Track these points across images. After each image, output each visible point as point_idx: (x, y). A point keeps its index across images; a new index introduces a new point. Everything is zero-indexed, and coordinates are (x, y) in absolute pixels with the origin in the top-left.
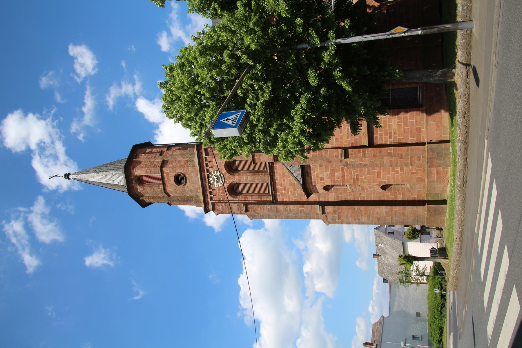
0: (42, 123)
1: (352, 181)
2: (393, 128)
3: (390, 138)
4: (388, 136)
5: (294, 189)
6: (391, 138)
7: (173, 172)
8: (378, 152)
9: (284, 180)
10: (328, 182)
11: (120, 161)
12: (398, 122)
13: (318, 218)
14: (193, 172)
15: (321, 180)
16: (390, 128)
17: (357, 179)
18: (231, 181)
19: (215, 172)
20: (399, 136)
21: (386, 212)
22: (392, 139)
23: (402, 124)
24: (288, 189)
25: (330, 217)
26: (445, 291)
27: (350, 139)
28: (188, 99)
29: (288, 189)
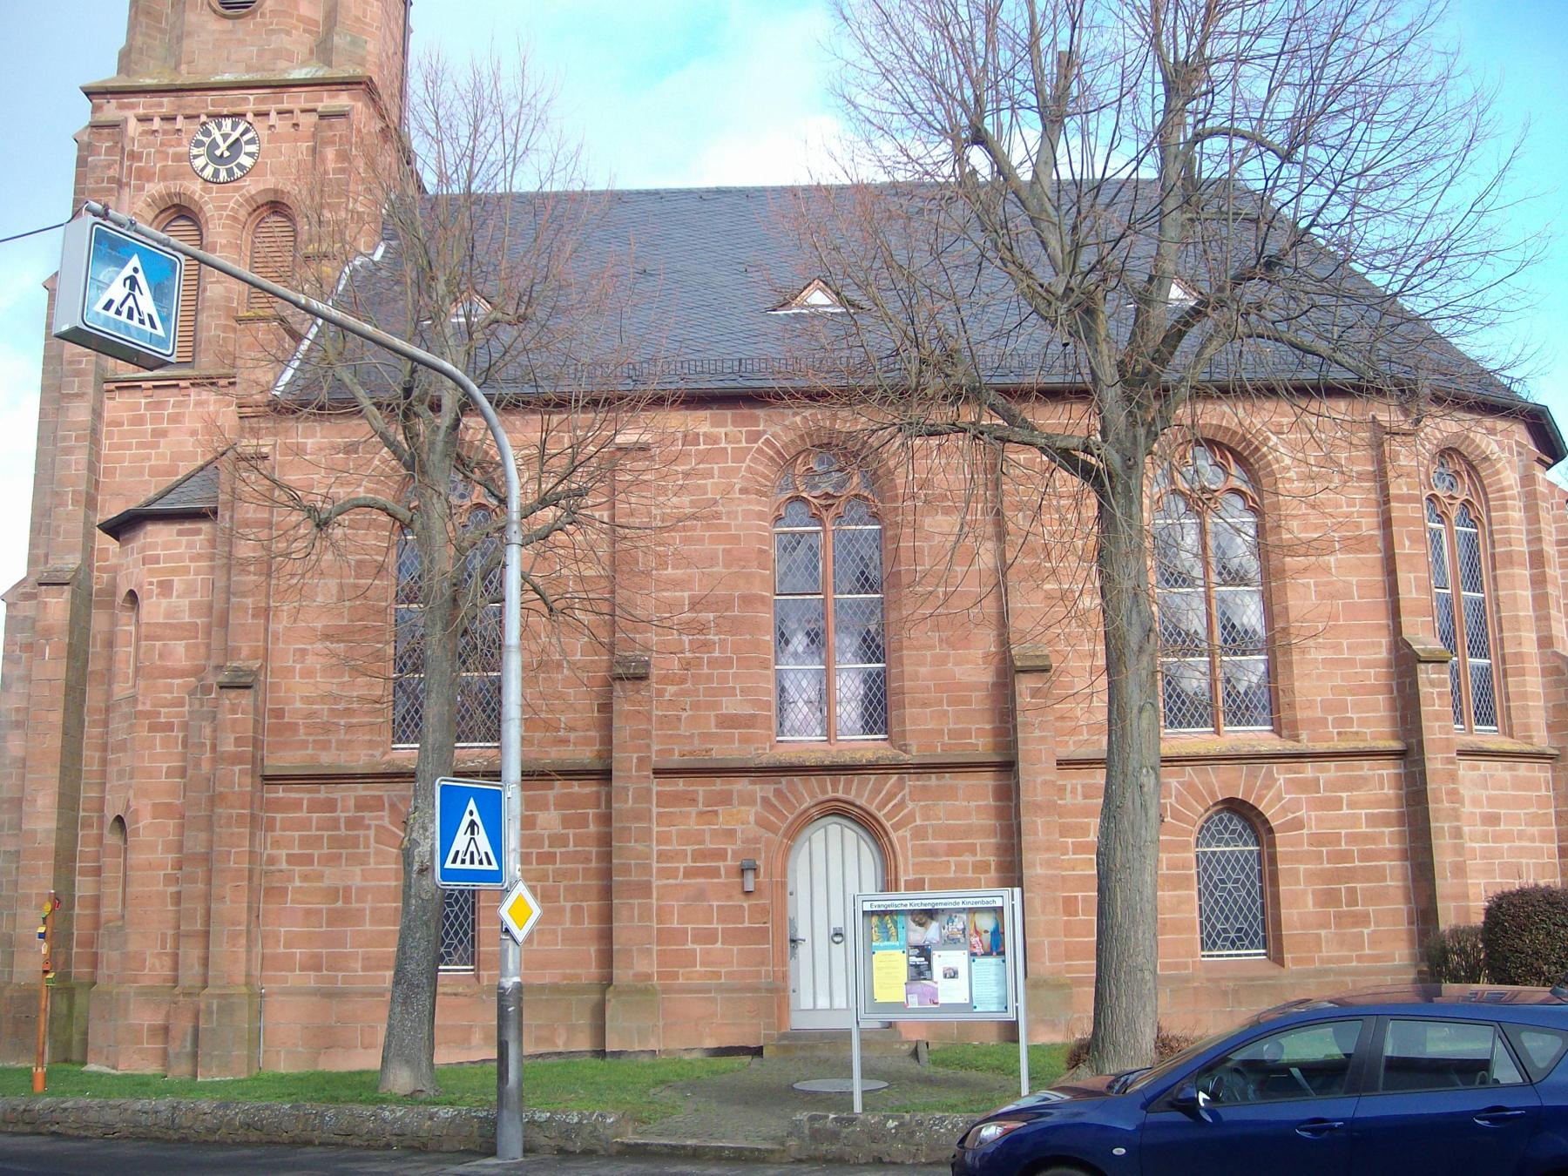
0: (1409, 988)
1: (148, 707)
2: (327, 870)
3: (291, 859)
4: (296, 851)
5: (154, 472)
6: (289, 862)
8: (234, 812)
9: (194, 433)
13: (32, 561)
14: (261, 53)
15: (161, 584)
18: (209, 210)
19: (252, 148)
20: (297, 890)
21: (33, 833)
22: (284, 866)
23: (340, 904)
24: (156, 446)
25: (27, 608)
27: (298, 705)
29: (156, 446)
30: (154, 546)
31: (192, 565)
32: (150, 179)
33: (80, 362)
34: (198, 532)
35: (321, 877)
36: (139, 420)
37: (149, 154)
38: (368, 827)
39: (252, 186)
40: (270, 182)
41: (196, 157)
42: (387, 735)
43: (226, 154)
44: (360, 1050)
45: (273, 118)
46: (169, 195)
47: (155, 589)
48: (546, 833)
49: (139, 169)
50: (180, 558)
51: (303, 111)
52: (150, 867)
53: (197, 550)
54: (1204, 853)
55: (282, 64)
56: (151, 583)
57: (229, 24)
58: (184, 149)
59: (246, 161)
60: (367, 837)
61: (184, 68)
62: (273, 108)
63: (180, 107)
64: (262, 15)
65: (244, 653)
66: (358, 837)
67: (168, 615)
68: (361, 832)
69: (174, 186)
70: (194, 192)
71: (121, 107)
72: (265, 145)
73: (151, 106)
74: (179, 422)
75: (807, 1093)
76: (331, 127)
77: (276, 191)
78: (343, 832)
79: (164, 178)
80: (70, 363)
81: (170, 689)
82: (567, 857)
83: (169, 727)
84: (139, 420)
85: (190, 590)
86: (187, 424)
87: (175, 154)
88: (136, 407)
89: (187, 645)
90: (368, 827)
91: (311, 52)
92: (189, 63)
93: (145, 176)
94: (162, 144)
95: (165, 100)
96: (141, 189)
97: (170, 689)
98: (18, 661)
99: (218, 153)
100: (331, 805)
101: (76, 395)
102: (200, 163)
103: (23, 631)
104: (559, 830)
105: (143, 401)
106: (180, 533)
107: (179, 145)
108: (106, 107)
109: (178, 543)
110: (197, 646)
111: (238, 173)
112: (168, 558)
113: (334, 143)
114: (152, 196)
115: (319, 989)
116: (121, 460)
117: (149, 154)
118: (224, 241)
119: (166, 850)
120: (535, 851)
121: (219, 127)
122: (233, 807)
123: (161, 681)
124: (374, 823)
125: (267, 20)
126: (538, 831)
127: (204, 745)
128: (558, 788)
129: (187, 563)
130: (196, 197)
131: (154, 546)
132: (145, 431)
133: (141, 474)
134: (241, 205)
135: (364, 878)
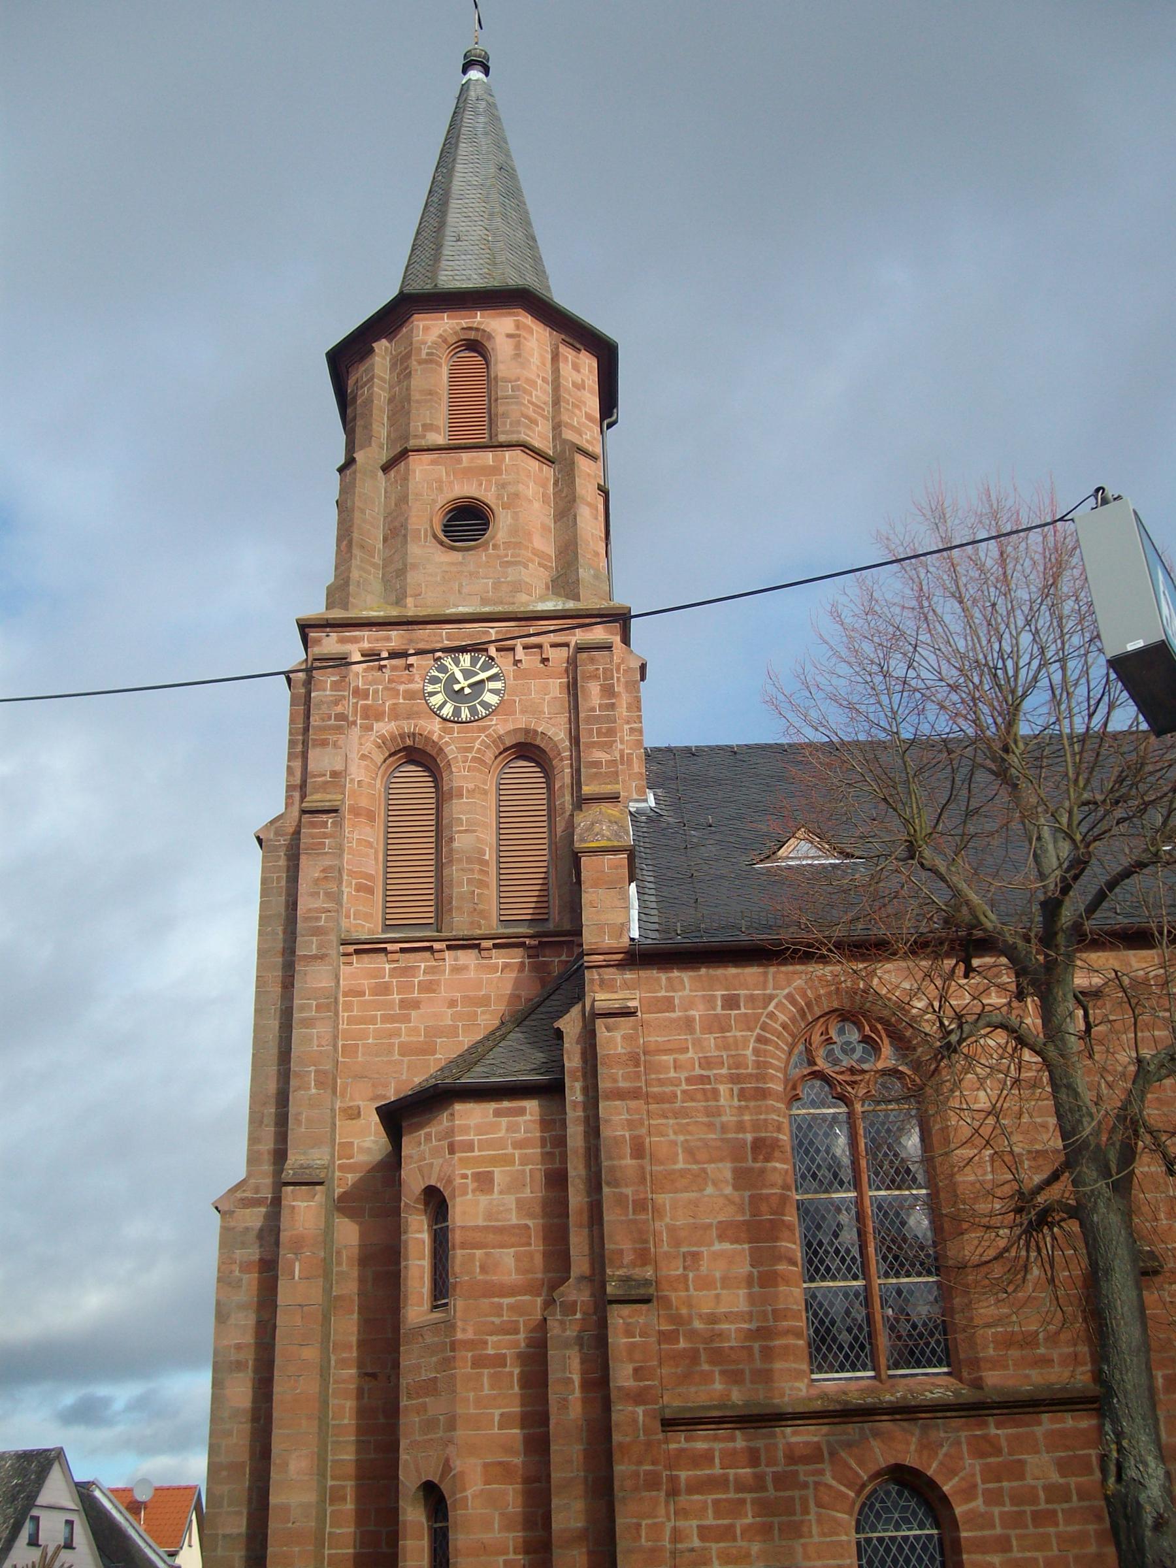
1: (470, 1335)
5: (405, 1050)
6: (702, 1538)
7: (499, 497)
9: (452, 1003)
10: (467, 1211)
11: (540, 271)
14: (497, 585)
15: (477, 1177)
18: (451, 751)
19: (498, 685)
21: (286, 1508)
22: (696, 1543)
26: (1101, 889)
28: (1046, 1230)
30: (465, 1129)
31: (517, 1152)
32: (379, 717)
33: (318, 919)
34: (522, 1112)
36: (384, 989)
37: (376, 692)
38: (805, 1485)
39: (501, 726)
40: (521, 721)
41: (432, 694)
43: (467, 691)
45: (520, 653)
46: (402, 736)
47: (471, 1184)
48: (1040, 1483)
49: (366, 709)
51: (553, 645)
52: (484, 1549)
53: (521, 1135)
54: (868, 1541)
55: (524, 598)
56: (465, 1176)
57: (458, 556)
58: (416, 686)
59: (492, 699)
61: (410, 601)
63: (411, 641)
64: (495, 547)
65: (628, 1258)
66: (792, 1498)
67: (489, 1216)
68: (796, 1493)
69: (408, 726)
70: (432, 732)
71: (342, 641)
72: (511, 682)
73: (377, 640)
74: (434, 991)
76: (592, 660)
77: (527, 731)
78: (771, 1493)
79: (395, 715)
80: (306, 919)
82: (1070, 1515)
83: (500, 1360)
84: (384, 989)
85: (515, 1185)
86: (444, 993)
87: (405, 691)
88: (379, 973)
91: (547, 588)
92: (416, 595)
93: (372, 715)
94: (390, 681)
95: (393, 633)
96: (370, 728)
98: (238, 1285)
99: (457, 687)
102: (436, 700)
103: (243, 1245)
104: (1055, 1478)
105: (387, 966)
106: (497, 1113)
107: (411, 681)
108: (325, 641)
109: (494, 1127)
110: (531, 1255)
111: (482, 711)
112: (483, 1145)
113: (597, 677)
114: (382, 737)
116: (364, 1035)
117: (376, 692)
118: (471, 786)
120: (1028, 1509)
121: (457, 662)
124: (811, 1479)
125: (502, 552)
126: (1029, 1481)
127: (570, 1380)
128: (1048, 1423)
129: (510, 1150)
130: (435, 738)
131: (465, 1129)
133: (390, 1052)
134: (488, 747)
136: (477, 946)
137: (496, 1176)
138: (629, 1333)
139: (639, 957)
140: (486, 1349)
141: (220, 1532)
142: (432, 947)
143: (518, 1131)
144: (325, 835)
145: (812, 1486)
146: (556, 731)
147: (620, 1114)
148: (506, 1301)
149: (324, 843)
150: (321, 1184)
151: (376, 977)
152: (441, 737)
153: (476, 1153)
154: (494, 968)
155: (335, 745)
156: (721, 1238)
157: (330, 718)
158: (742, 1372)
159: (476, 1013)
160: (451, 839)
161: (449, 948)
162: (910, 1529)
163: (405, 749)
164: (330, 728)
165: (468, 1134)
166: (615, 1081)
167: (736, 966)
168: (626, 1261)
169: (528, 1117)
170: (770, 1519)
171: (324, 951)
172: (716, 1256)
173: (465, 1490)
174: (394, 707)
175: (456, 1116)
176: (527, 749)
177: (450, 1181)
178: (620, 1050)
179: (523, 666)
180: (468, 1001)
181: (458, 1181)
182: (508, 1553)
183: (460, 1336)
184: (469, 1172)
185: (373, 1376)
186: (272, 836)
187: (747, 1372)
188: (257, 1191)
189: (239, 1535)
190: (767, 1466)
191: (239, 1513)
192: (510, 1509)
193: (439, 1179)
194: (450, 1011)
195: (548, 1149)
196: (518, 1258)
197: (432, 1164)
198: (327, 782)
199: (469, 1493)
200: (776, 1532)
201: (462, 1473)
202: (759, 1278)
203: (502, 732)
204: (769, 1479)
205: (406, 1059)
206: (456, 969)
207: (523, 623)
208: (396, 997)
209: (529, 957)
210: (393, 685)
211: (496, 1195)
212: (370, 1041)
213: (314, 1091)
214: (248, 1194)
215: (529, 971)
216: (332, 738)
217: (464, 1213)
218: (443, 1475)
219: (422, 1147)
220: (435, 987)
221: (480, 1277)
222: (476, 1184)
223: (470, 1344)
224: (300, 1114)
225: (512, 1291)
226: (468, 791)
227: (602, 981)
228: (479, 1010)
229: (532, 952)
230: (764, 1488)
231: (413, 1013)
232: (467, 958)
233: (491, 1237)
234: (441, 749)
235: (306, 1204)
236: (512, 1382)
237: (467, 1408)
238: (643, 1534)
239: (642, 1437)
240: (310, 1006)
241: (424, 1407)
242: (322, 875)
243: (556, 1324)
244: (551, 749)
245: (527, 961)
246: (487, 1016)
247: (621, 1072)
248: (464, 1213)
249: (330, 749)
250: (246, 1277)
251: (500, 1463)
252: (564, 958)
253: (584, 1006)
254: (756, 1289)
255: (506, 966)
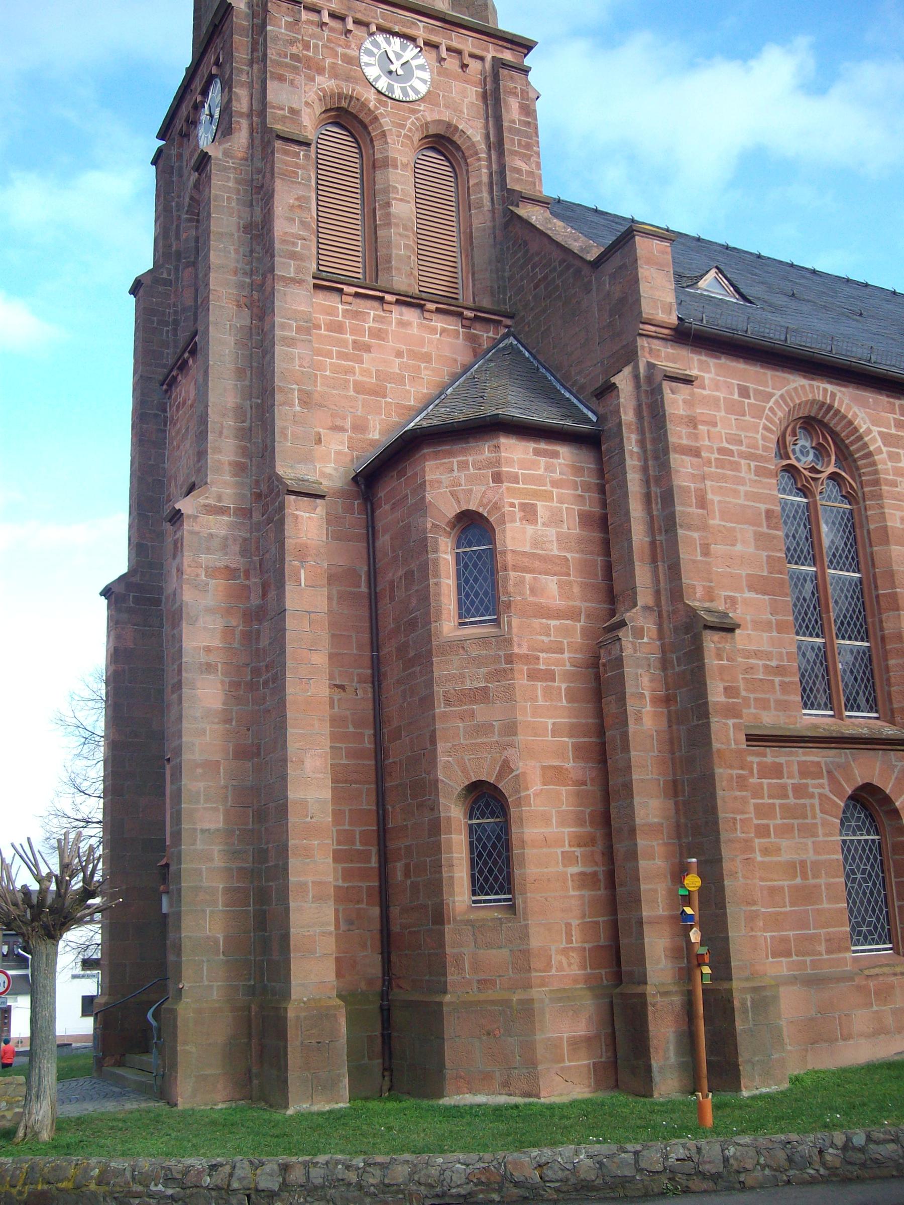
1: (524, 650)
2: (784, 843)
5: (360, 388)
8: (735, 772)
9: (399, 354)
10: (515, 537)
12: (803, 863)
15: (523, 507)
16: (784, 831)
17: (533, 675)
21: (304, 803)
30: (510, 462)
31: (555, 491)
32: (320, 71)
34: (555, 455)
35: (778, 850)
36: (338, 328)
38: (812, 796)
42: (796, 698)
44: (841, 1043)
46: (340, 96)
50: (539, 480)
52: (545, 842)
53: (557, 476)
56: (512, 505)
60: (813, 806)
62: (444, 43)
65: (699, 592)
67: (535, 544)
69: (347, 88)
75: (447, 1109)
77: (449, 125)
78: (792, 801)
79: (335, 75)
81: (546, 631)
83: (549, 676)
84: (338, 328)
85: (555, 520)
89: (559, 580)
90: (812, 796)
97: (546, 631)
100: (777, 771)
101: (293, 280)
103: (208, 550)
105: (340, 306)
106: (537, 452)
107: (348, 47)
109: (534, 465)
112: (528, 479)
115: (795, 977)
119: (562, 823)
122: (731, 767)
123: (536, 622)
124: (816, 791)
131: (510, 462)
132: (345, 341)
133: (346, 388)
135: (816, 852)
136: (421, 307)
137: (539, 509)
138: (719, 657)
139: (684, 335)
140: (538, 664)
141: (198, 827)
142: (383, 297)
143: (555, 472)
144: (297, 166)
145: (817, 797)
146: (473, 131)
147: (684, 467)
148: (553, 623)
149: (297, 173)
150: (322, 497)
151: (328, 314)
152: (377, 108)
153: (521, 486)
154: (433, 330)
155: (292, 83)
156: (751, 588)
157: (286, 56)
158: (768, 700)
159: (419, 367)
160: (388, 204)
161: (398, 302)
162: (862, 835)
163: (339, 109)
164: (287, 66)
165: (513, 467)
166: (680, 437)
167: (746, 363)
168: (698, 595)
169: (561, 461)
170: (792, 821)
171: (301, 276)
172: (746, 602)
173: (527, 789)
174: (334, 66)
175: (502, 448)
176: (441, 142)
177: (496, 507)
178: (681, 412)
179: (446, 65)
180: (413, 354)
181: (507, 508)
182: (781, 805)
183: (516, 650)
184: (516, 502)
185: (342, 687)
186: (220, 156)
187: (772, 700)
188: (219, 498)
189: (218, 830)
190: (788, 778)
191: (216, 809)
192: (564, 808)
193: (481, 504)
194: (397, 360)
195: (579, 492)
196: (560, 585)
197: (471, 490)
198: (284, 117)
199: (531, 792)
200: (796, 832)
201: (524, 773)
202: (777, 624)
203: (429, 119)
204: (790, 788)
205: (361, 397)
206: (401, 324)
207: (447, 26)
208: (349, 337)
209: (463, 326)
210: (332, 45)
211: (539, 526)
212: (328, 373)
213: (298, 408)
214: (211, 501)
215: (464, 339)
216: (289, 76)
217: (513, 538)
218: (500, 776)
219: (456, 473)
220: (383, 335)
221: (531, 599)
222: (523, 514)
223: (526, 659)
224: (286, 428)
225: (558, 614)
226: (401, 163)
227: (651, 349)
228: (423, 365)
229: (466, 322)
230: (786, 796)
231: (365, 356)
232: (411, 315)
233: (537, 564)
234: (376, 119)
235: (308, 515)
236: (561, 696)
237: (525, 715)
238: (738, 827)
239: (733, 746)
240: (290, 326)
241: (472, 714)
242: (297, 203)
243: (630, 646)
244: (468, 148)
245: (461, 330)
246: (428, 372)
247: (684, 431)
248: (513, 538)
249: (286, 85)
250: (212, 582)
251: (554, 767)
252: (491, 334)
253: (636, 368)
254: (775, 634)
255: (443, 331)
